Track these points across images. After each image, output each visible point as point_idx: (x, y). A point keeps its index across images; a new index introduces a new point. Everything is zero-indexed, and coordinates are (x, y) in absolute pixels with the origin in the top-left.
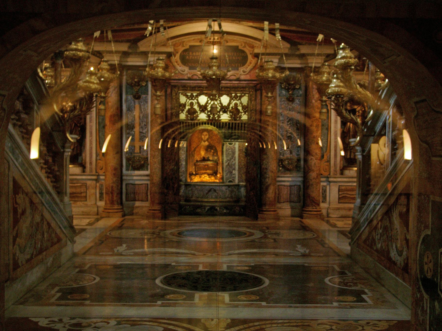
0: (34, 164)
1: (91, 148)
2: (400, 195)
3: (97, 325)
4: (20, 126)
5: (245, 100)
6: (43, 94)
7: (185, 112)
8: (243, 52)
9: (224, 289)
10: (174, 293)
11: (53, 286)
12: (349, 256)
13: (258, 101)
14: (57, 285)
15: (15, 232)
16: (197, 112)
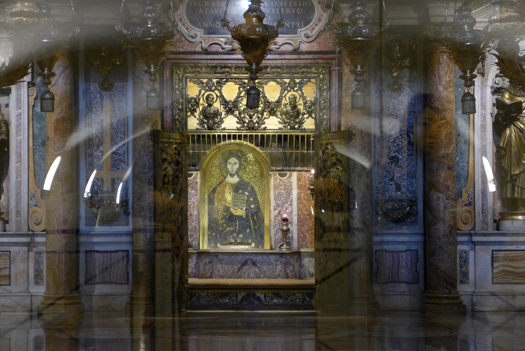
5: (310, 91)
7: (197, 114)
16: (221, 114)
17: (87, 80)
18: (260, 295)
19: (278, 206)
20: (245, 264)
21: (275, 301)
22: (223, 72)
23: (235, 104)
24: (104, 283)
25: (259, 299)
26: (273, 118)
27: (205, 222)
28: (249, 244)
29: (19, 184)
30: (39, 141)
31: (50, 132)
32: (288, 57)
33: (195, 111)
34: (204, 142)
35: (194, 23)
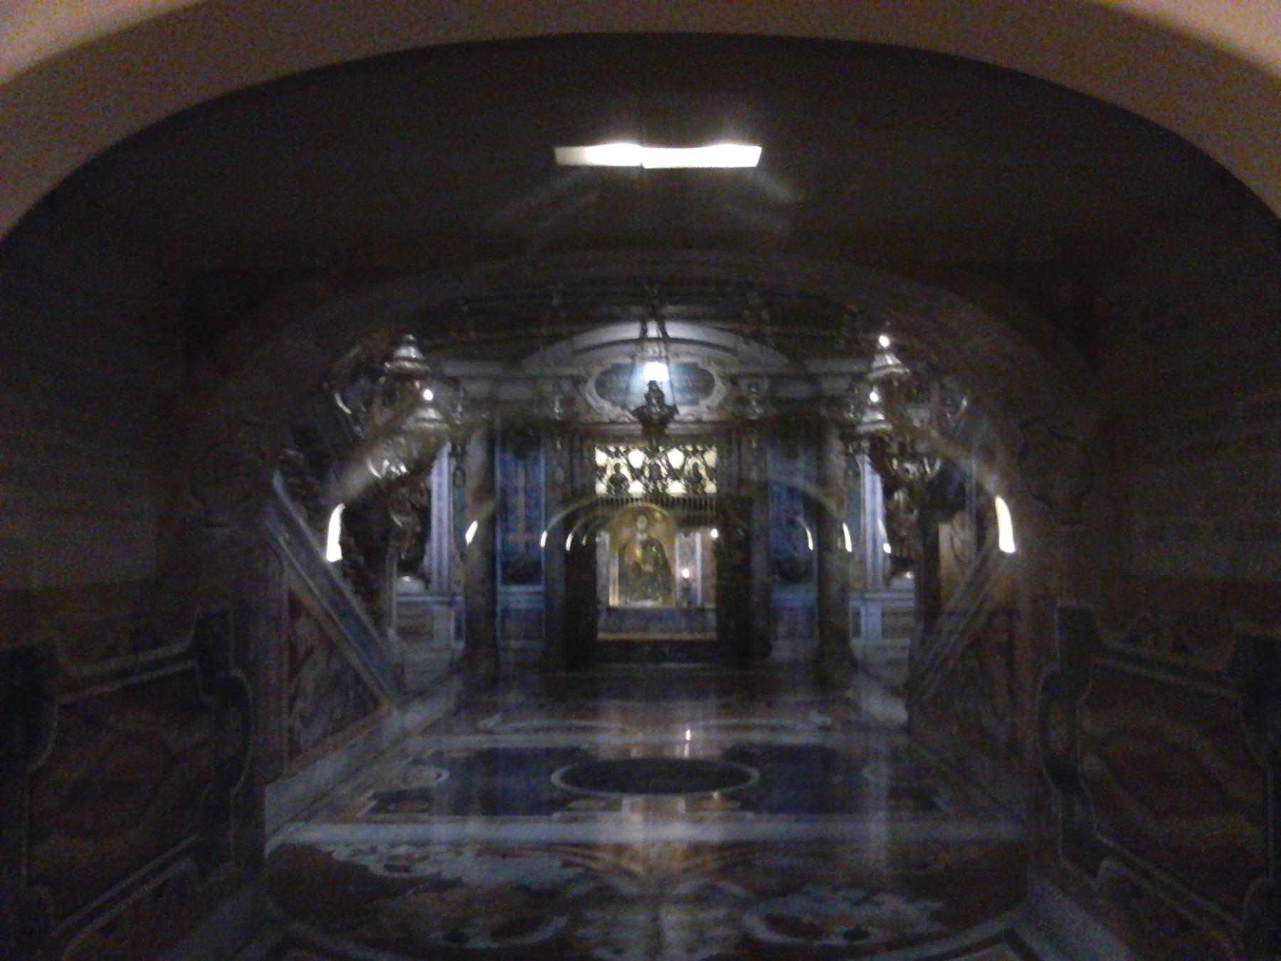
0: (336, 575)
1: (440, 539)
2: (994, 614)
3: (439, 858)
4: (304, 498)
5: (711, 457)
6: (350, 448)
8: (707, 372)
9: (676, 790)
10: (588, 797)
11: (362, 789)
12: (907, 729)
13: (735, 457)
14: (370, 787)
15: (293, 688)
18: (666, 649)
22: (628, 440)
23: (641, 471)
27: (615, 571)
28: (656, 599)
29: (440, 546)
31: (469, 500)
35: (602, 396)
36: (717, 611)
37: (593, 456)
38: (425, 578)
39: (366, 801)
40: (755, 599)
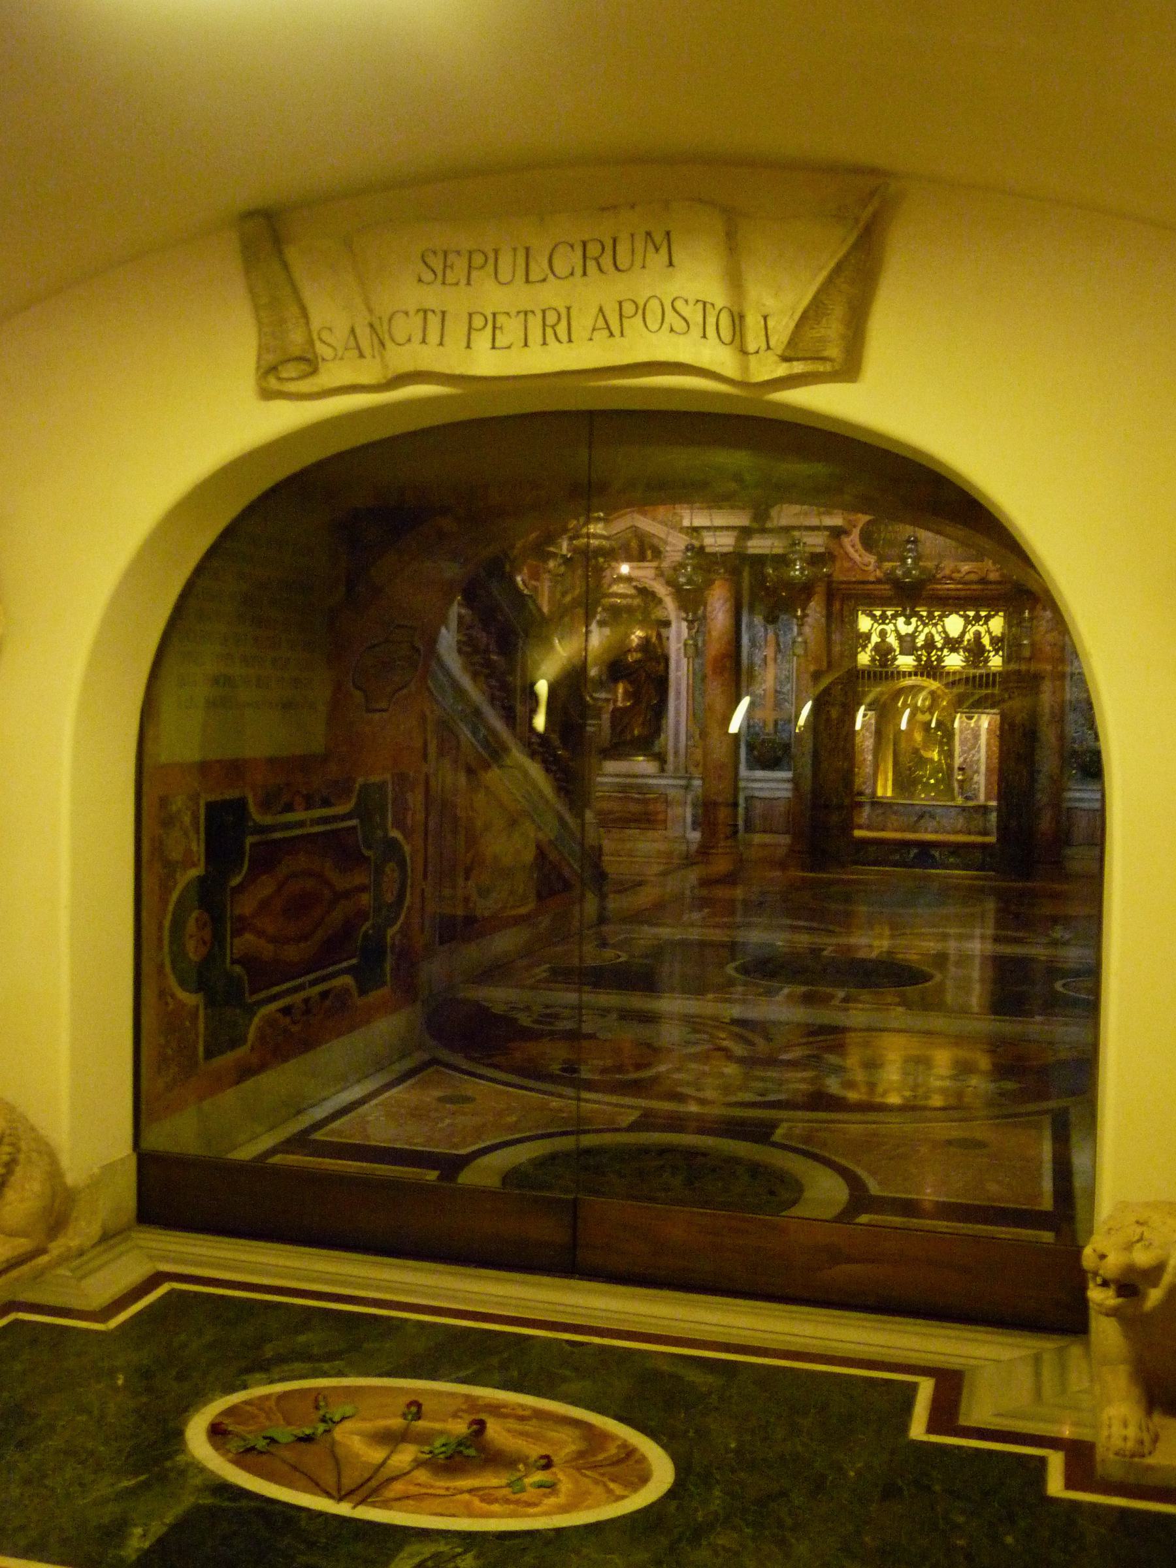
5: (997, 625)
7: (868, 650)
10: (198, 840)
17: (752, 610)
19: (963, 752)
20: (921, 817)
21: (951, 860)
24: (764, 832)
25: (933, 857)
26: (954, 655)
29: (677, 723)
30: (699, 675)
31: (709, 671)
32: (974, 587)
33: (866, 646)
34: (863, 678)
36: (999, 809)
37: (855, 621)
38: (661, 758)
39: (541, 972)
40: (1042, 798)
